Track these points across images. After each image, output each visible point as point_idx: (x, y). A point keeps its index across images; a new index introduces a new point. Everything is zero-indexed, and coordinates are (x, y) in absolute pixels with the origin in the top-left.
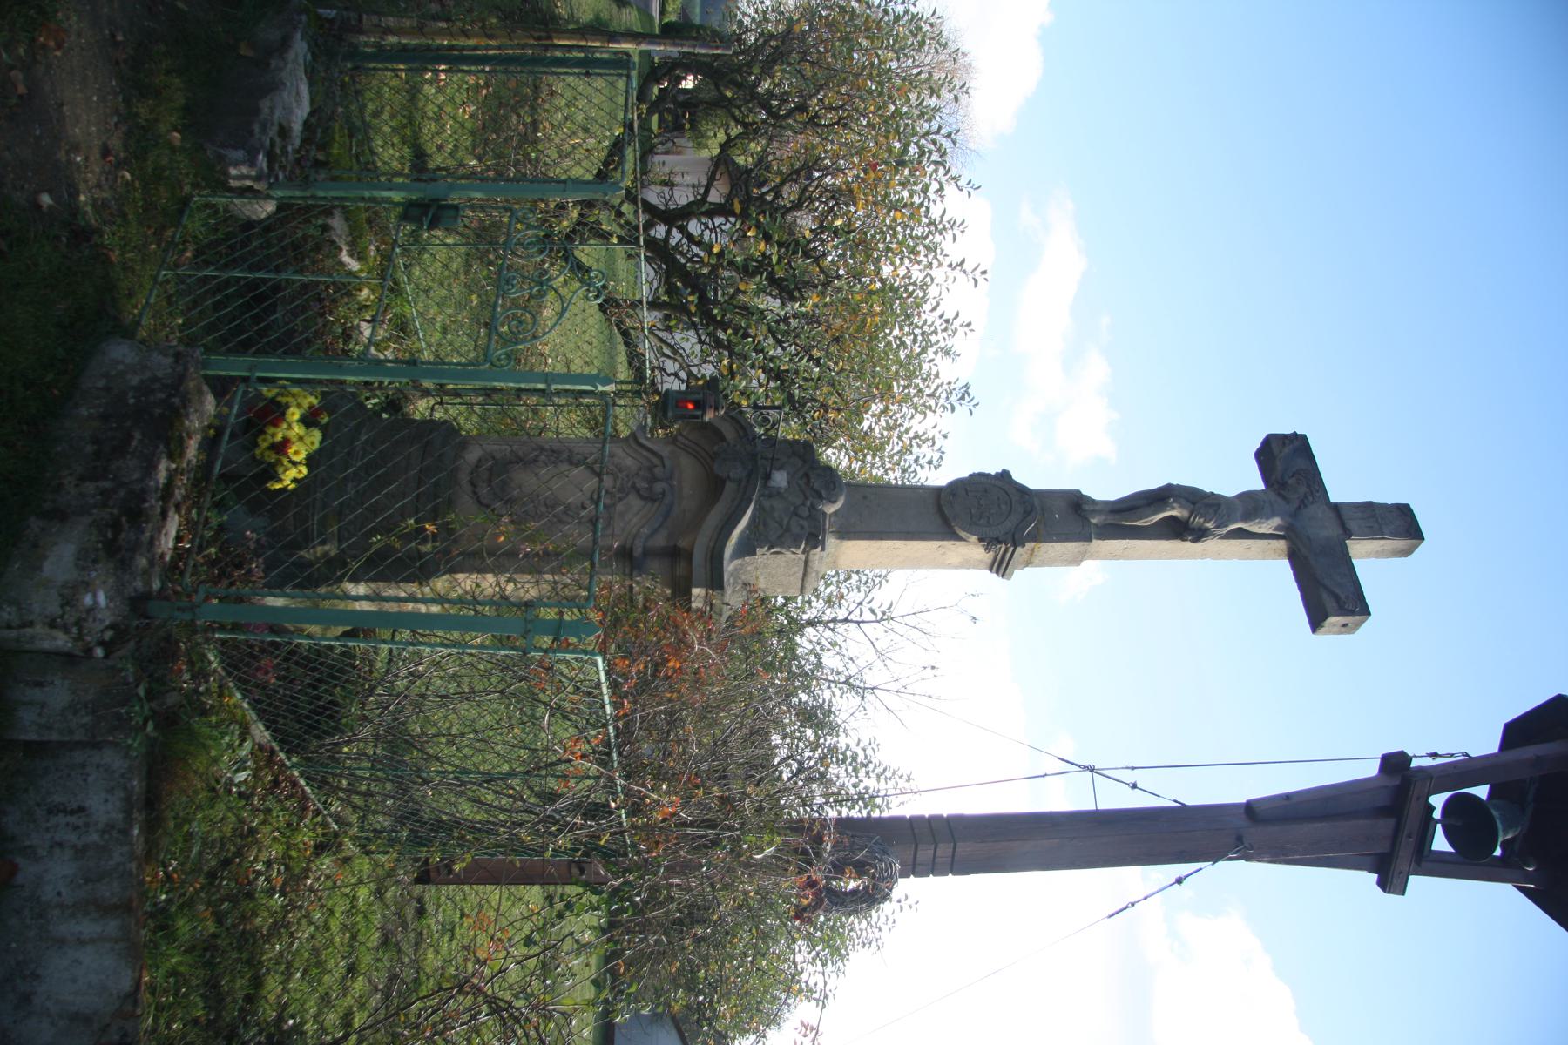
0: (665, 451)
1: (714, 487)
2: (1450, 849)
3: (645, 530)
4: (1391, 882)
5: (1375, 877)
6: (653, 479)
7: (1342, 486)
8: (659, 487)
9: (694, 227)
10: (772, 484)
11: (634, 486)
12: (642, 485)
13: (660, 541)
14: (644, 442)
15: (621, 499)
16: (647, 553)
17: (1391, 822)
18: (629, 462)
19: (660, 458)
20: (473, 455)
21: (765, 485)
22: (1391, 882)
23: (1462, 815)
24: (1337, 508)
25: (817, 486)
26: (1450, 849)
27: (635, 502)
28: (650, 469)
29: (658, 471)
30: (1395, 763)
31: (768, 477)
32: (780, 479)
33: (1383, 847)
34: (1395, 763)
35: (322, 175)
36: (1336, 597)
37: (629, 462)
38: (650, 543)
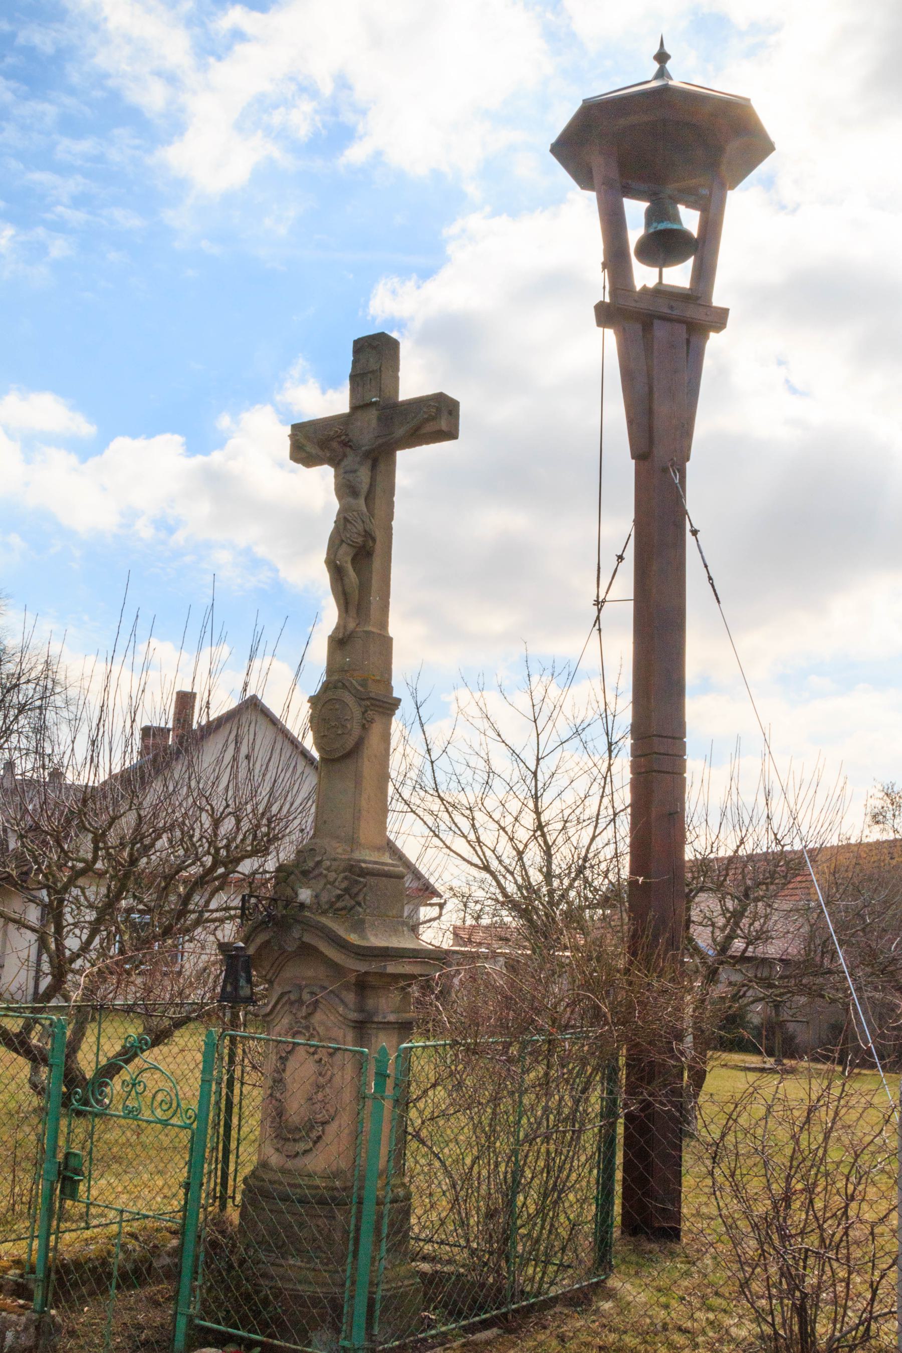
0: (278, 990)
1: (307, 951)
2: (693, 258)
3: (341, 1009)
4: (719, 319)
5: (712, 335)
6: (300, 1001)
7: (336, 402)
8: (306, 997)
9: (72, 943)
10: (308, 901)
11: (305, 1018)
12: (304, 1011)
13: (350, 997)
14: (270, 1007)
15: (314, 1029)
16: (361, 1009)
17: (657, 323)
18: (285, 1021)
19: (283, 995)
20: (275, 1159)
21: (309, 908)
22: (719, 319)
23: (664, 244)
24: (355, 408)
25: (311, 864)
26: (693, 258)
27: (318, 1017)
28: (292, 1003)
29: (293, 997)
30: (606, 315)
31: (302, 906)
32: (305, 895)
33: (681, 330)
34: (606, 315)
35: (686, 426)
36: (427, 420)
37: (285, 1021)
38: (351, 1006)
